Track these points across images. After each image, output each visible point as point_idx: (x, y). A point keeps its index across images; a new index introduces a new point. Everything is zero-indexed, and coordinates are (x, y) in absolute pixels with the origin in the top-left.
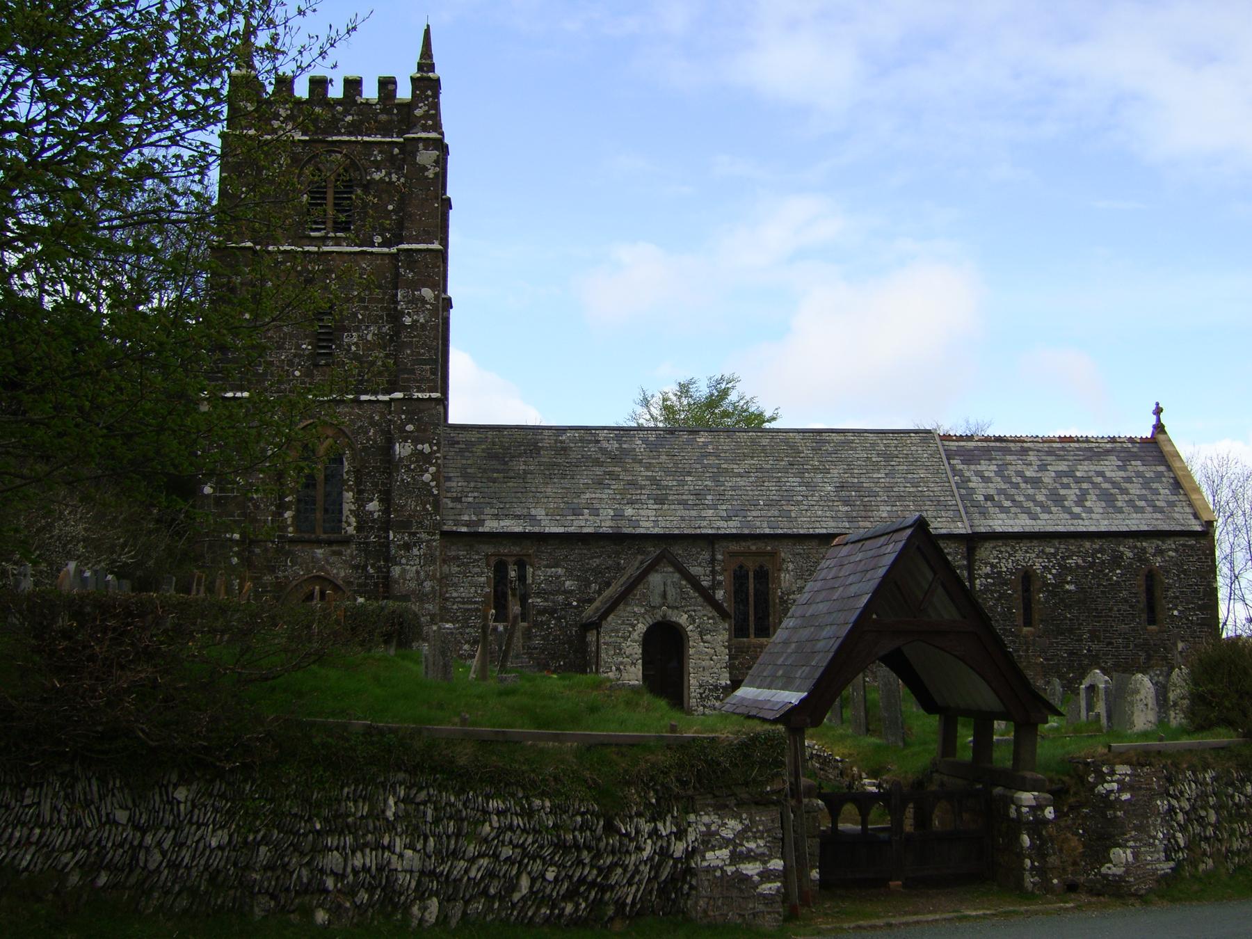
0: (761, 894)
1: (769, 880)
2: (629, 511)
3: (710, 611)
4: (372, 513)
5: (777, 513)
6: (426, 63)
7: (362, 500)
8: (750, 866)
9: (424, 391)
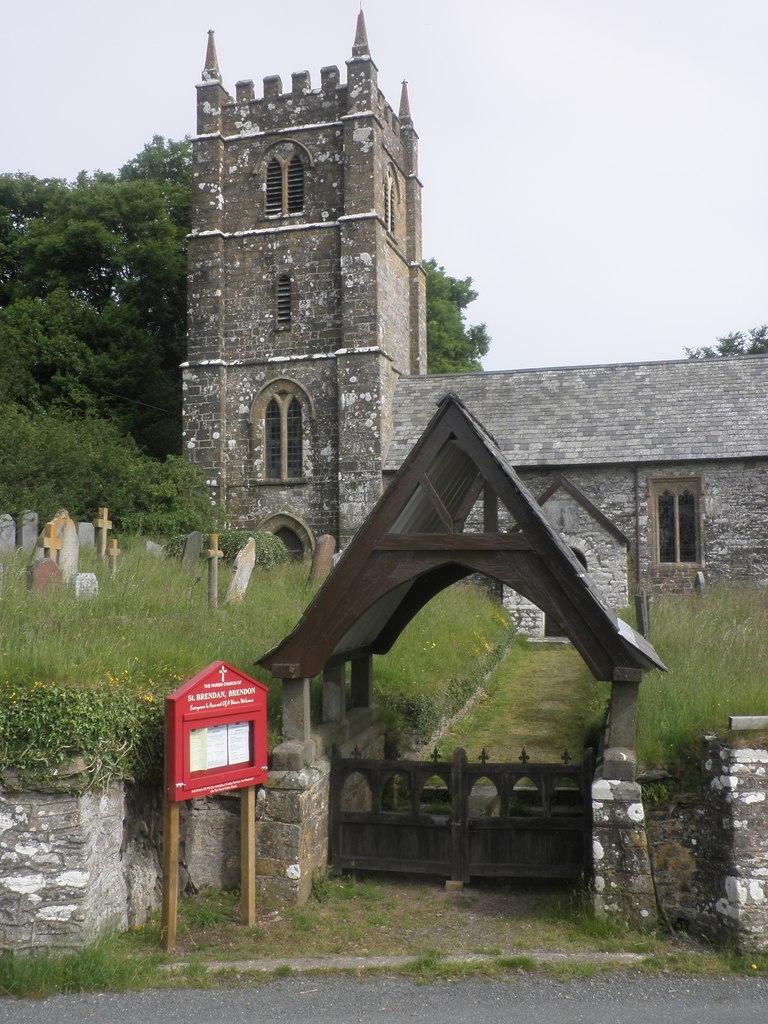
0: (42, 921)
1: (56, 901)
2: (557, 444)
3: (605, 536)
4: (325, 457)
5: (703, 439)
6: (361, 47)
7: (318, 446)
8: (27, 879)
9: (365, 345)
